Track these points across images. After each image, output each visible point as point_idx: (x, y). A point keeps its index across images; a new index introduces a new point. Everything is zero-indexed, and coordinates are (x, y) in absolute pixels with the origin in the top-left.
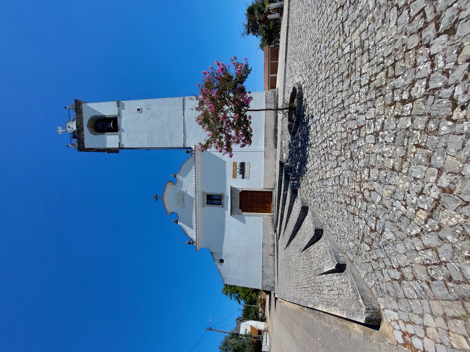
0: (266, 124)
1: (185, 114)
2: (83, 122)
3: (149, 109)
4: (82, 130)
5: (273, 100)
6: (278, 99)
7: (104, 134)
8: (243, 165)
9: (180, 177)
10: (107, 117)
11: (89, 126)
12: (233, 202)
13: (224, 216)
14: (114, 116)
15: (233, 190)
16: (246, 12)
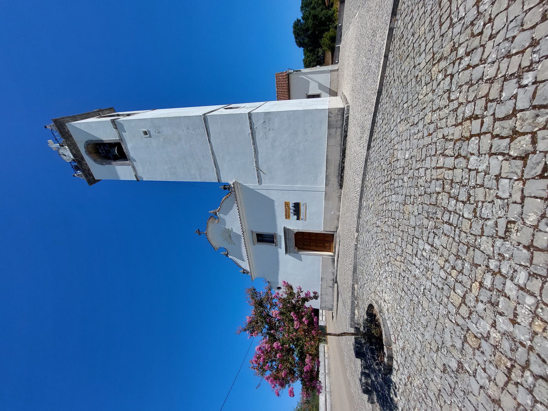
0: (328, 157)
1: (211, 140)
2: (78, 148)
3: (159, 132)
4: (82, 158)
5: (340, 123)
6: (347, 124)
7: (110, 164)
8: (297, 206)
9: (221, 215)
10: (105, 142)
11: (89, 153)
12: (287, 242)
13: (277, 254)
14: (116, 142)
15: (287, 231)
16: (293, 25)
